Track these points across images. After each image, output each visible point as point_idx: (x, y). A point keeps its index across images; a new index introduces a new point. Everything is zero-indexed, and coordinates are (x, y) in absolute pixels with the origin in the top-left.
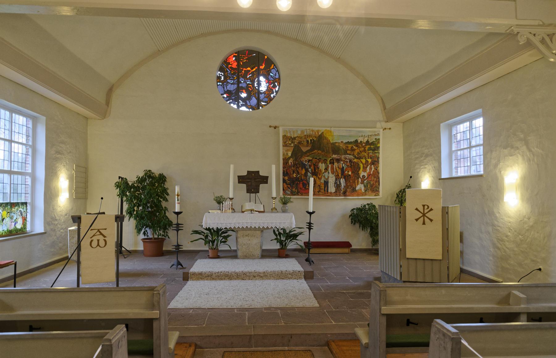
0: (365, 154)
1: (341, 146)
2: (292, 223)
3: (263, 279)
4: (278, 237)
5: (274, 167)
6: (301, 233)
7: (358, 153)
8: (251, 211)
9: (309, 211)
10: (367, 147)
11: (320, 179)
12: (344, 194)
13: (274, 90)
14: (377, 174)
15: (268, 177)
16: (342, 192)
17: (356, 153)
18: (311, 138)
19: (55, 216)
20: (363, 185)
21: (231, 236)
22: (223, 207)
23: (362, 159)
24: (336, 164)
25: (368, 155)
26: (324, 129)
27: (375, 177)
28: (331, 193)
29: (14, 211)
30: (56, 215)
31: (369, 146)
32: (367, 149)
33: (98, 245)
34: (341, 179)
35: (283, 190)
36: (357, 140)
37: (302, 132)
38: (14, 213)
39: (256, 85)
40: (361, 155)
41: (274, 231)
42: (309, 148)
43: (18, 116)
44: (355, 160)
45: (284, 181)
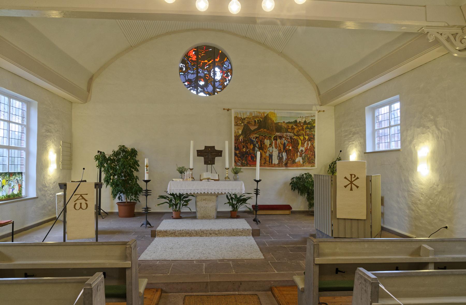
0: (303, 132)
1: (283, 125)
2: (242, 190)
3: (218, 236)
4: (231, 201)
5: (227, 143)
6: (249, 198)
7: (297, 131)
8: (208, 179)
10: (305, 126)
11: (265, 153)
13: (227, 79)
15: (222, 151)
16: (284, 164)
18: (258, 119)
19: (45, 183)
20: (301, 158)
21: (191, 200)
23: (301, 136)
24: (279, 141)
26: (269, 111)
27: (311, 151)
28: (275, 164)
29: (12, 179)
30: (46, 183)
31: (307, 126)
32: (304, 128)
33: (81, 207)
34: (283, 153)
35: (235, 162)
36: (296, 120)
37: (251, 113)
38: (12, 181)
39: (212, 75)
40: (300, 133)
41: (227, 196)
42: (256, 127)
44: (295, 137)
45: (236, 155)
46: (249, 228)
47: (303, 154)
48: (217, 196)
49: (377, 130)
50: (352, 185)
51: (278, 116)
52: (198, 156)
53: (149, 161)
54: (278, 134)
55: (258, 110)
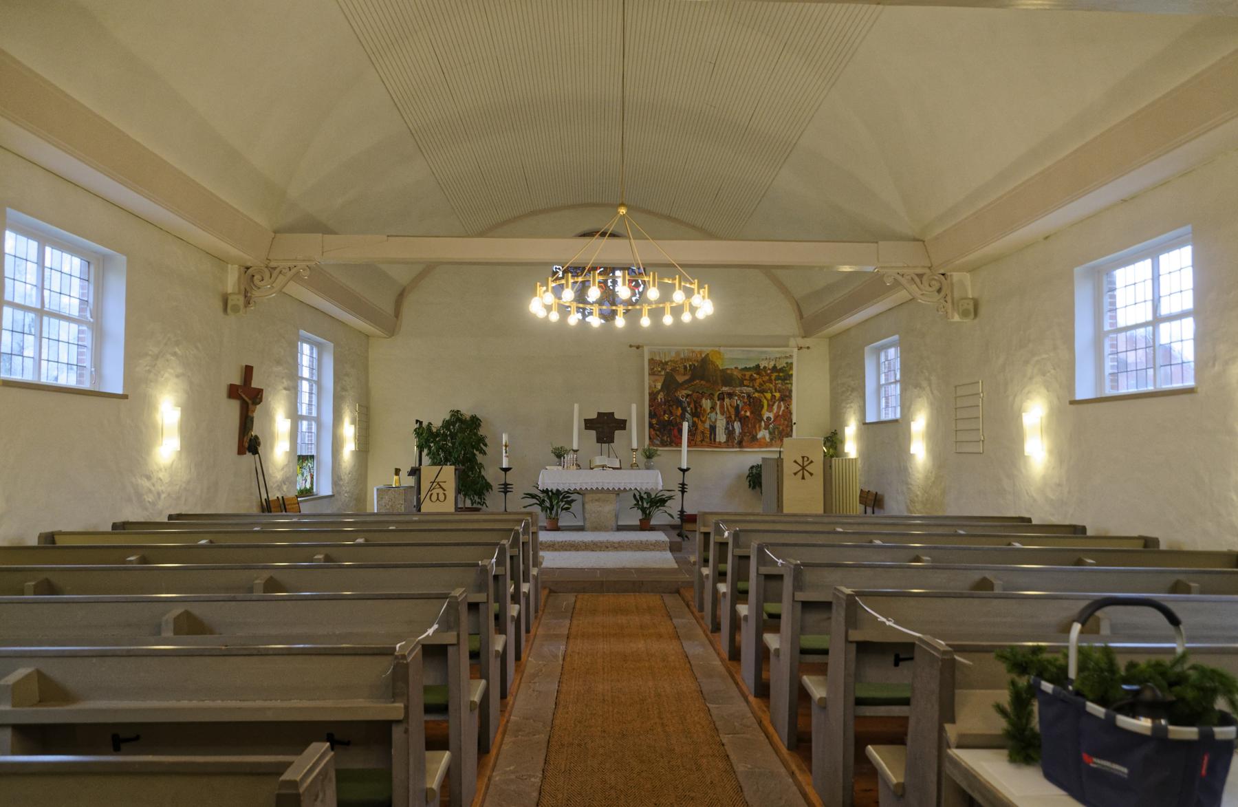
0: (771, 385)
1: (735, 373)
2: (657, 484)
3: (617, 551)
4: (640, 503)
5: (634, 407)
6: (670, 498)
7: (761, 384)
8: (603, 467)
9: (682, 468)
10: (775, 375)
11: (703, 422)
12: (740, 444)
13: (637, 291)
14: (789, 415)
15: (625, 421)
16: (736, 441)
17: (758, 384)
18: (691, 363)
20: (767, 431)
21: (576, 500)
22: (564, 462)
23: (767, 392)
24: (727, 401)
25: (775, 386)
26: (710, 349)
27: (785, 420)
28: (720, 443)
31: (777, 374)
32: (773, 378)
33: (438, 499)
34: (735, 423)
35: (650, 438)
36: (759, 365)
37: (678, 353)
39: (609, 284)
40: (764, 387)
41: (635, 495)
42: (687, 377)
43: (69, 256)
44: (757, 395)
45: (651, 425)
46: (667, 539)
47: (771, 424)
48: (618, 494)
49: (883, 385)
50: (805, 472)
51: (726, 357)
52: (586, 429)
53: (510, 437)
54: (725, 389)
55: (690, 348)
